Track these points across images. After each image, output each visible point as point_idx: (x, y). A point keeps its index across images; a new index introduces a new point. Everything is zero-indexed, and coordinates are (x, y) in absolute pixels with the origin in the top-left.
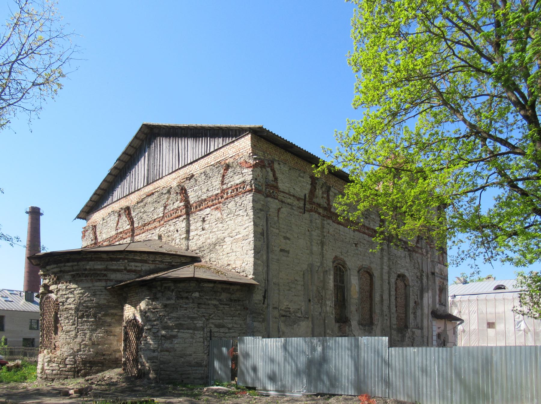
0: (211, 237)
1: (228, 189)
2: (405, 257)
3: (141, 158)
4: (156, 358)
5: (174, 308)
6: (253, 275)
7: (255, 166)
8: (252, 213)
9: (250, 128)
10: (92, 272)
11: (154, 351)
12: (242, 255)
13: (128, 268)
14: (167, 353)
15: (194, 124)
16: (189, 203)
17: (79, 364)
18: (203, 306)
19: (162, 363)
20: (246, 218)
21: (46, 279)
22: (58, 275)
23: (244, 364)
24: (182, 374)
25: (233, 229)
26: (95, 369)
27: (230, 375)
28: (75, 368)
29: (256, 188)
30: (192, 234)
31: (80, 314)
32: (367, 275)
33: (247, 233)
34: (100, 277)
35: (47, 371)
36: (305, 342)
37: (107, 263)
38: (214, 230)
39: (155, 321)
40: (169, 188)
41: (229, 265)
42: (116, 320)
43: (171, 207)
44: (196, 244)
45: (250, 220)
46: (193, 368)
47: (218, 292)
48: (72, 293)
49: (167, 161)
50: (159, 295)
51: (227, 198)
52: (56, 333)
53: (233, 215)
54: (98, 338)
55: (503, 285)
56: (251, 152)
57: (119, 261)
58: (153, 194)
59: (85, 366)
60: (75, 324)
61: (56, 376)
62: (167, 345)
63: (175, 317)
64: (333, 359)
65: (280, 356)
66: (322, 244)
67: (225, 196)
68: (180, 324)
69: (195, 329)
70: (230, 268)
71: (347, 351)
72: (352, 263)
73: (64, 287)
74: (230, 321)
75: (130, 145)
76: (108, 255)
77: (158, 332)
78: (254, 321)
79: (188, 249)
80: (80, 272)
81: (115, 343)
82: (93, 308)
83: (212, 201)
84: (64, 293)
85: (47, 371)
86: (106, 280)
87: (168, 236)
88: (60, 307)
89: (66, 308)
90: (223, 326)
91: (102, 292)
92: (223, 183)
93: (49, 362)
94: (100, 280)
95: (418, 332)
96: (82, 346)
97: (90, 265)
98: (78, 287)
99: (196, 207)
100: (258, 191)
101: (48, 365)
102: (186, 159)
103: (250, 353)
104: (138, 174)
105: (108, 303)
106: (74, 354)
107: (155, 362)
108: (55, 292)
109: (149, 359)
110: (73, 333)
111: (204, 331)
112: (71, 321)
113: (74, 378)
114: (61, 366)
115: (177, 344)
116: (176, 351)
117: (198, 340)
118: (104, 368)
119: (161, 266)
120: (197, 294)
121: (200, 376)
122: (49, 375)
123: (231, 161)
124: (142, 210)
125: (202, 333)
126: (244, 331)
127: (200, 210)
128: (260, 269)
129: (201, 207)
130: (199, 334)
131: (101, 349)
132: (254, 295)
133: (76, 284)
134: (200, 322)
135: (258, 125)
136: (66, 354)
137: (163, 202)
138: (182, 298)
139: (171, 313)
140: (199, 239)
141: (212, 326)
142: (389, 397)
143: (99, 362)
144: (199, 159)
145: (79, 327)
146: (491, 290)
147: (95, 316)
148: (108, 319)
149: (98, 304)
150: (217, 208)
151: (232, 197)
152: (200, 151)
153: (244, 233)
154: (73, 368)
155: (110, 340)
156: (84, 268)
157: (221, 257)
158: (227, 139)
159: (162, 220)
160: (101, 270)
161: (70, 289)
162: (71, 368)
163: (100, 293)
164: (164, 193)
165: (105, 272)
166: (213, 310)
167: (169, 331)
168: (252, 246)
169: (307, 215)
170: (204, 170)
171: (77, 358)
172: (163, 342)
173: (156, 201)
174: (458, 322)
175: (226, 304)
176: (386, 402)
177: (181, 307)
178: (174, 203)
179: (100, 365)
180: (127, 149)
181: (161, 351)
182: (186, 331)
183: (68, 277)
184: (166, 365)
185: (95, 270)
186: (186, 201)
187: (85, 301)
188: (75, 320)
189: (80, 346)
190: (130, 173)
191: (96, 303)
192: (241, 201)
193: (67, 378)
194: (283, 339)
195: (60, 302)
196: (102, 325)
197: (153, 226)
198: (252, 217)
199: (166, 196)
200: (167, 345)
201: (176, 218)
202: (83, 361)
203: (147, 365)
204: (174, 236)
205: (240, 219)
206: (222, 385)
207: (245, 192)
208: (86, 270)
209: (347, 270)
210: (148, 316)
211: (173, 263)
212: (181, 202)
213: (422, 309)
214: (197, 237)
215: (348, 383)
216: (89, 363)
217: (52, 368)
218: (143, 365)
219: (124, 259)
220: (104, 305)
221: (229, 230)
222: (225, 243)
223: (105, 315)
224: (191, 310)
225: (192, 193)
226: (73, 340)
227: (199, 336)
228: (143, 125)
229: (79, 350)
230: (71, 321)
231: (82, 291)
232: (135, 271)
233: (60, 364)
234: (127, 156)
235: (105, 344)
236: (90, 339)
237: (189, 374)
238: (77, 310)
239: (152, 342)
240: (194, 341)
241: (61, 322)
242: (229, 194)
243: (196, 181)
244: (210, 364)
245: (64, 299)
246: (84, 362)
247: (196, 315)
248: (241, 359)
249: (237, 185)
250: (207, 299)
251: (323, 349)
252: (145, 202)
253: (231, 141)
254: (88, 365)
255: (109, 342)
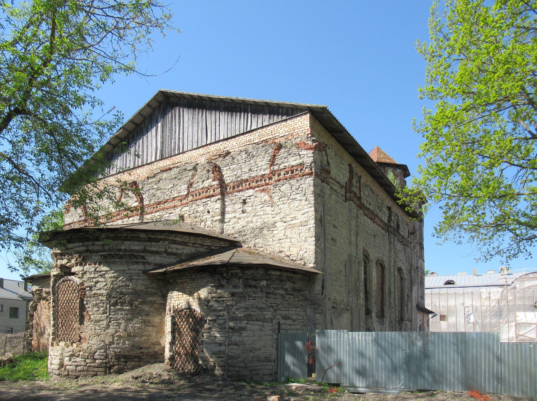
0: (254, 220)
1: (281, 170)
2: (402, 251)
3: (152, 128)
4: (223, 352)
5: (243, 297)
6: (314, 263)
7: (315, 148)
8: (313, 198)
9: (309, 107)
10: (128, 253)
11: (220, 345)
12: (298, 242)
13: (169, 250)
14: (236, 347)
15: (234, 97)
16: (224, 182)
17: (111, 358)
18: (272, 296)
19: (230, 357)
20: (304, 203)
21: (62, 259)
22: (84, 255)
23: (324, 358)
24: (251, 370)
25: (288, 213)
26: (130, 364)
27: (306, 370)
28: (106, 363)
29: (316, 172)
30: (227, 216)
31: (113, 301)
32: (380, 267)
33: (307, 219)
34: (137, 259)
35: (67, 367)
36: (402, 336)
37: (145, 243)
38: (258, 214)
39: (220, 311)
40: (194, 164)
41: (281, 252)
42: (155, 309)
43: (198, 186)
44: (233, 228)
45: (310, 206)
46: (263, 364)
47: (284, 280)
48: (102, 276)
49: (190, 134)
50: (224, 282)
51: (279, 180)
52: (81, 322)
53: (287, 199)
54: (134, 329)
55: (452, 281)
56: (309, 132)
57: (159, 242)
58: (170, 169)
59: (118, 361)
60: (106, 313)
61: (82, 373)
62: (236, 338)
63: (243, 307)
64: (436, 354)
65: (371, 350)
66: (357, 234)
67: (276, 178)
68: (249, 315)
69: (264, 320)
70: (282, 255)
71: (452, 347)
72: (373, 256)
73: (93, 269)
74: (294, 312)
75: (140, 113)
76: (147, 235)
77: (224, 323)
78: (316, 313)
79: (223, 232)
80: (113, 253)
81: (154, 335)
82: (128, 294)
83: (257, 181)
84: (92, 276)
85: (67, 367)
86: (144, 263)
87: (196, 217)
88: (87, 293)
89: (95, 294)
90: (289, 318)
91: (139, 276)
92: (272, 163)
93: (71, 356)
94: (137, 263)
95: (408, 323)
96: (115, 338)
97: (126, 245)
98: (111, 270)
99: (234, 188)
100: (317, 175)
101: (70, 360)
102: (217, 134)
103: (332, 346)
104: (147, 146)
105: (147, 289)
106: (105, 348)
107: (222, 357)
108: (80, 275)
109: (213, 354)
110: (105, 323)
111: (272, 323)
112: (102, 309)
113: (106, 374)
114: (88, 361)
115: (247, 337)
116: (245, 344)
117: (267, 333)
118: (142, 363)
119: (202, 250)
120: (264, 283)
121: (269, 372)
122: (72, 371)
123: (282, 141)
124: (155, 187)
125: (271, 325)
126: (305, 323)
127: (240, 191)
128: (319, 257)
129: (240, 188)
130: (268, 326)
131: (138, 342)
132: (316, 285)
133: (108, 266)
134: (269, 313)
135: (321, 105)
136: (95, 347)
137: (187, 179)
138: (250, 286)
139: (239, 302)
140: (237, 222)
141: (280, 317)
142: (501, 394)
143: (135, 357)
144: (238, 136)
145: (111, 316)
146: (442, 284)
147: (131, 304)
148: (146, 308)
149: (135, 290)
150: (263, 190)
151: (286, 179)
152: (237, 126)
153: (301, 218)
154: (103, 363)
155: (148, 331)
156: (118, 248)
157: (270, 243)
158: (276, 116)
159: (184, 199)
160: (138, 251)
161: (100, 272)
162: (102, 363)
163: (138, 277)
164: (188, 169)
165: (143, 254)
166: (281, 301)
167: (238, 322)
168: (313, 232)
169: (347, 204)
170: (244, 148)
171: (108, 352)
172: (231, 334)
173: (176, 178)
174: (430, 316)
175: (291, 295)
176: (500, 398)
177: (249, 296)
178: (203, 181)
179: (136, 359)
180: (135, 117)
181: (229, 345)
182: (256, 322)
183: (96, 257)
184: (235, 360)
185: (131, 251)
186: (220, 180)
187: (119, 286)
188: (106, 308)
189: (113, 338)
190: (136, 144)
191: (132, 289)
192: (298, 185)
193: (96, 375)
194: (374, 333)
195: (87, 287)
196: (139, 314)
197: (172, 204)
198: (313, 202)
199: (191, 173)
200: (236, 338)
201: (206, 198)
202: (116, 355)
203: (211, 360)
204: (204, 218)
205: (296, 203)
206: (298, 382)
207: (304, 175)
208: (120, 250)
209: (369, 262)
210: (212, 306)
211: (213, 247)
212: (214, 180)
213: (412, 302)
214: (236, 220)
215: (454, 378)
216: (123, 358)
217: (76, 364)
218: (205, 360)
219: (165, 240)
220: (142, 291)
221: (282, 215)
222: (276, 229)
223: (142, 303)
224: (259, 300)
225: (228, 172)
226: (105, 330)
227: (268, 328)
228: (161, 92)
229: (113, 343)
230: (102, 309)
231: (116, 274)
232: (175, 254)
233: (88, 358)
234: (133, 125)
235: (143, 336)
236: (125, 330)
237: (259, 370)
238: (109, 296)
239: (218, 335)
240: (264, 334)
241: (88, 309)
242: (282, 176)
243: (233, 158)
244: (280, 359)
245: (93, 283)
246: (118, 357)
247: (265, 306)
248: (321, 354)
249: (293, 166)
250: (275, 288)
251: (424, 344)
252: (159, 177)
253: (280, 119)
254: (122, 360)
255: (147, 333)
